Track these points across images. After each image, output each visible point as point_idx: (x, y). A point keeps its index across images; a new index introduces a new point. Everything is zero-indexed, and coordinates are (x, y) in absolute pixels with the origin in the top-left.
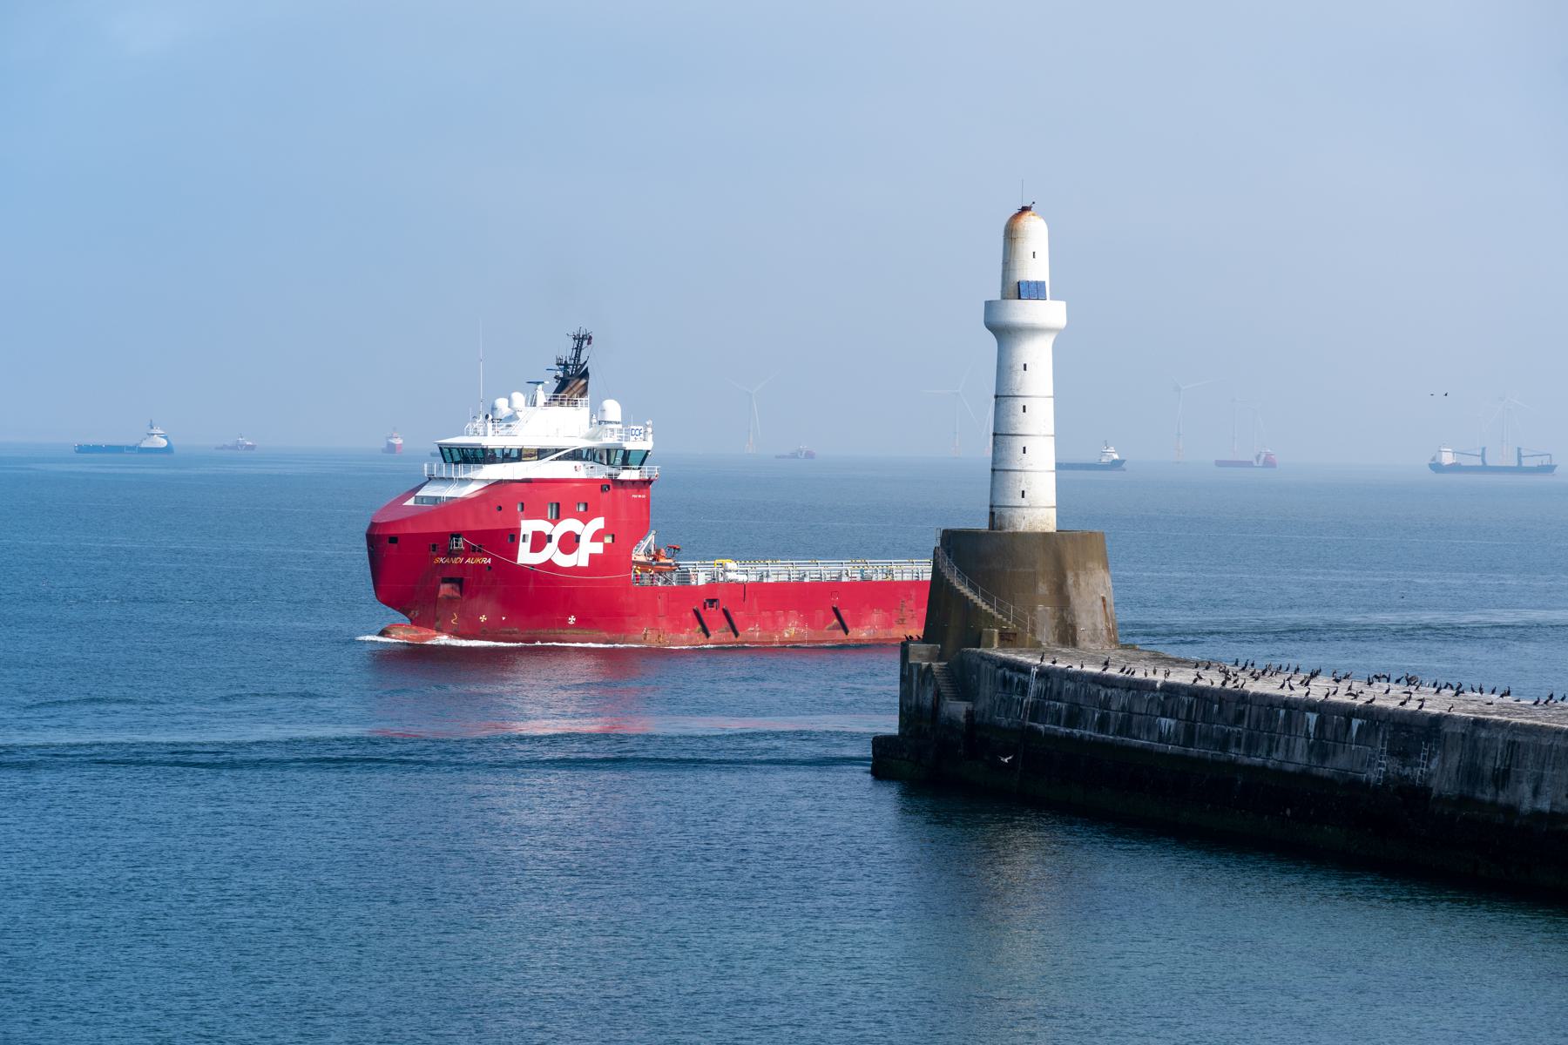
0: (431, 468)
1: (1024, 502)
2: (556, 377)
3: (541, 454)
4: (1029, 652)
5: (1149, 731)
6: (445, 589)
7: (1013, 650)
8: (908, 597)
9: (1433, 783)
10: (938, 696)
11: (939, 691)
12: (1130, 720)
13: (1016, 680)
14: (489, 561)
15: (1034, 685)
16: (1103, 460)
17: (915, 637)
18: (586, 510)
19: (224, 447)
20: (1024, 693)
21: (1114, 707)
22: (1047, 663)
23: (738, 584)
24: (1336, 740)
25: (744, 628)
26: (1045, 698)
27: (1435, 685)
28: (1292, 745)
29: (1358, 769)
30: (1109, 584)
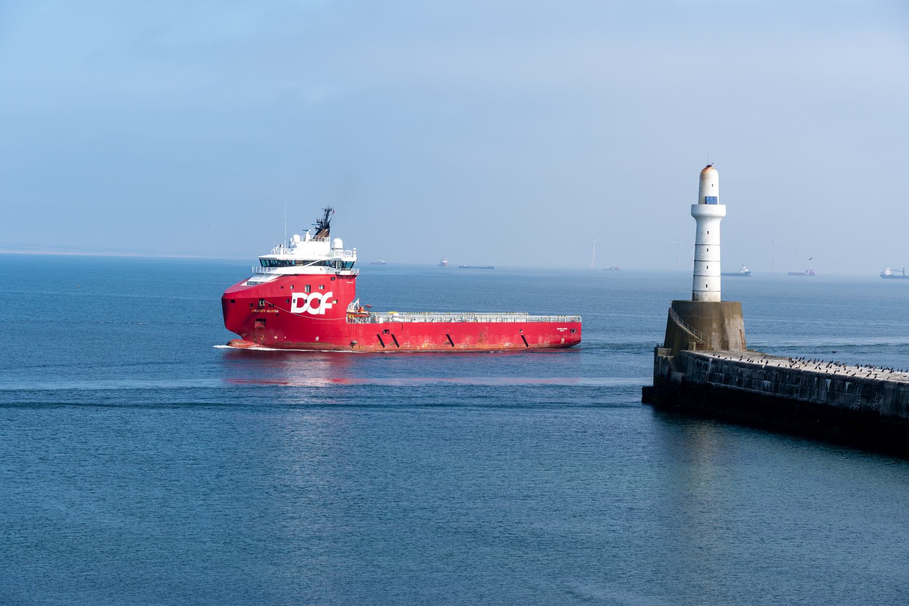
0: (255, 269)
1: (707, 289)
2: (316, 228)
3: (305, 263)
4: (709, 352)
5: (759, 386)
6: (257, 324)
7: (702, 351)
8: (484, 330)
9: (881, 409)
10: (670, 370)
11: (670, 368)
12: (751, 381)
13: (703, 364)
14: (278, 311)
15: (710, 366)
16: (741, 272)
17: (660, 345)
18: (324, 288)
19: (373, 263)
20: (706, 369)
21: (744, 376)
22: (716, 357)
23: (399, 323)
24: (839, 391)
25: (402, 344)
26: (715, 371)
27: (881, 368)
28: (820, 392)
29: (849, 403)
30: (743, 324)
